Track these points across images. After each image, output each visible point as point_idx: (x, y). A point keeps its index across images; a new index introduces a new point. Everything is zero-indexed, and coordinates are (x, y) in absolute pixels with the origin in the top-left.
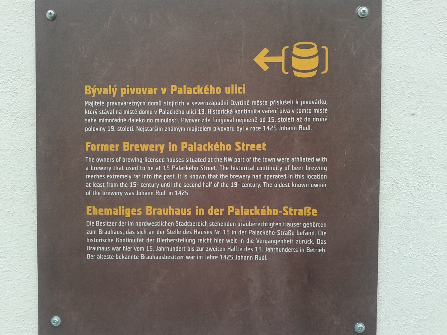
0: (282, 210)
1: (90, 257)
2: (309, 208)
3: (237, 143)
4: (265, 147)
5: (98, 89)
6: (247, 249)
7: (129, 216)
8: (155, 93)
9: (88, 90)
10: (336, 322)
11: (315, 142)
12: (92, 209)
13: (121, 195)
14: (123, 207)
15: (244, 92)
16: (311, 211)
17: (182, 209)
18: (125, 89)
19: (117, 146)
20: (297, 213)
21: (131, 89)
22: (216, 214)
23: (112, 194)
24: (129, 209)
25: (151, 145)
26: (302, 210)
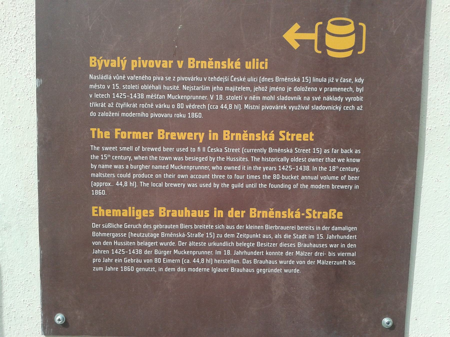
2: (335, 211)
3: (281, 133)
4: (313, 137)
5: (105, 61)
8: (170, 67)
9: (93, 61)
11: (343, 129)
12: (98, 209)
13: (351, 188)
15: (266, 68)
16: (336, 214)
18: (136, 61)
19: (151, 133)
20: (321, 215)
21: (143, 61)
23: (342, 187)
24: (140, 211)
25: (189, 134)
26: (326, 213)
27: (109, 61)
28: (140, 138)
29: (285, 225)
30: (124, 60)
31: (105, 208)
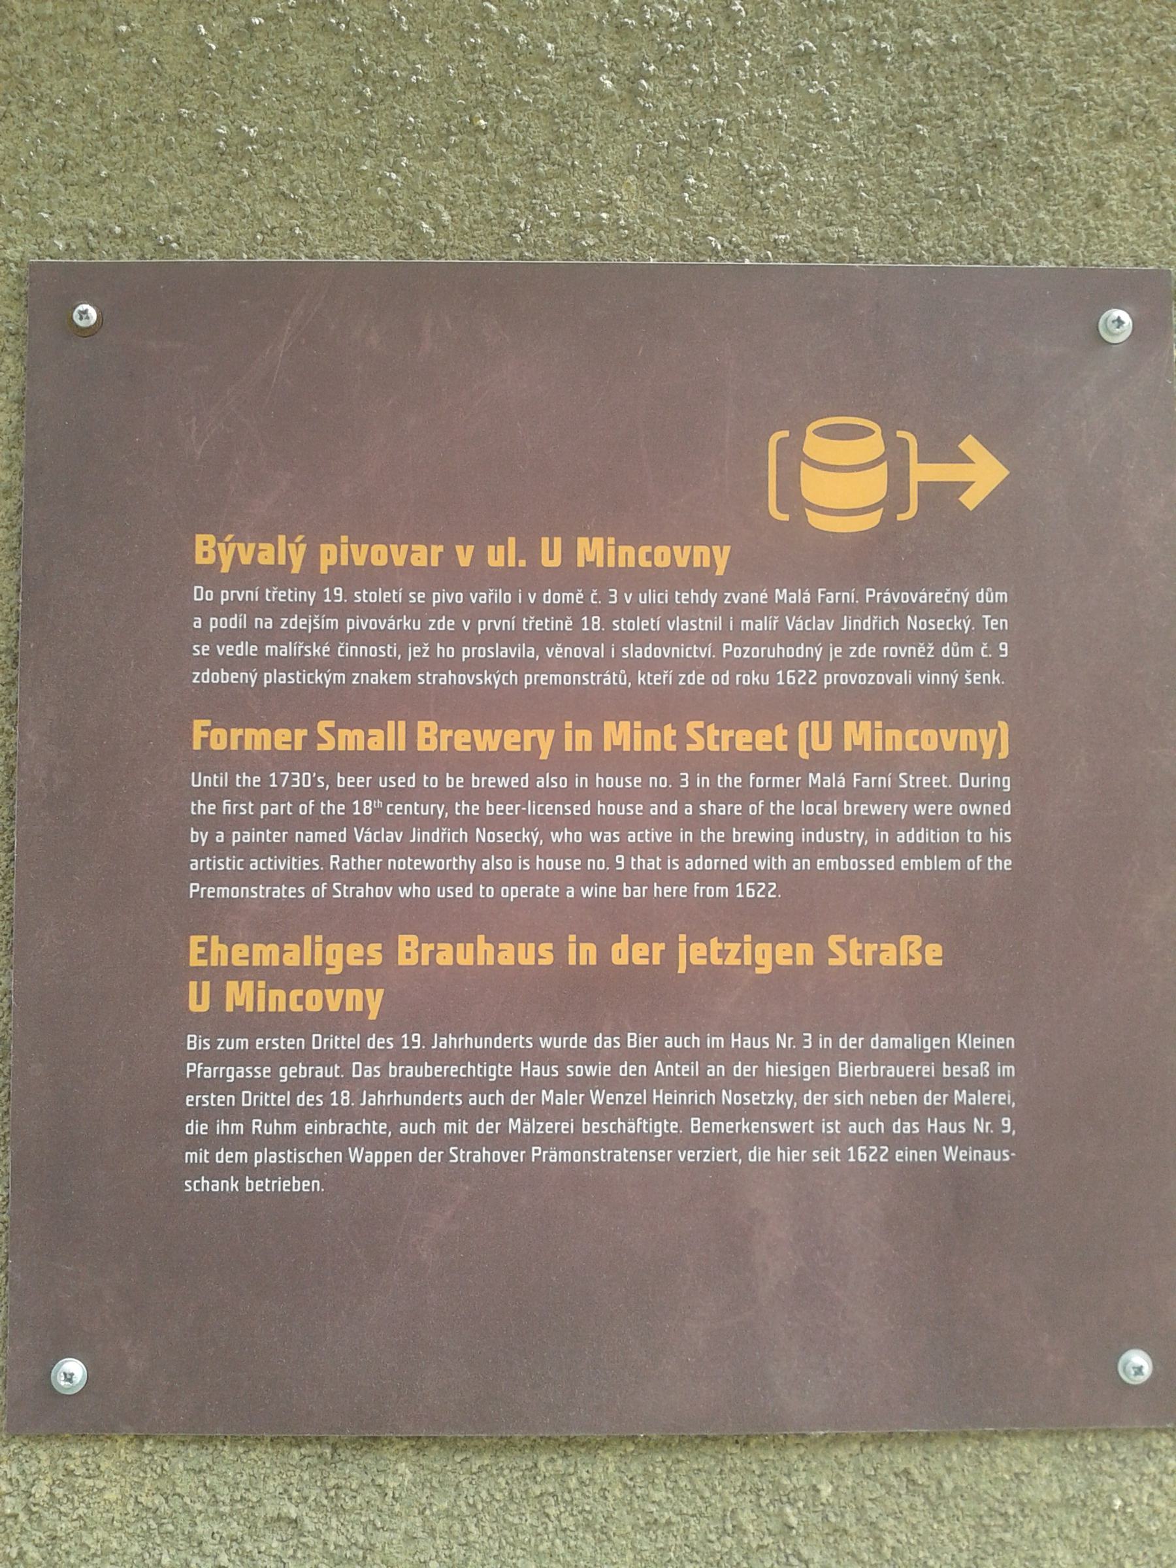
5: (241, 546)
6: (627, 1070)
7: (338, 970)
9: (206, 549)
12: (207, 945)
14: (319, 938)
16: (922, 950)
18: (332, 548)
20: (876, 954)
21: (354, 547)
22: (637, 961)
24: (768, 947)
25: (508, 733)
26: (892, 947)
27: (252, 546)
30: (297, 545)
31: (229, 941)
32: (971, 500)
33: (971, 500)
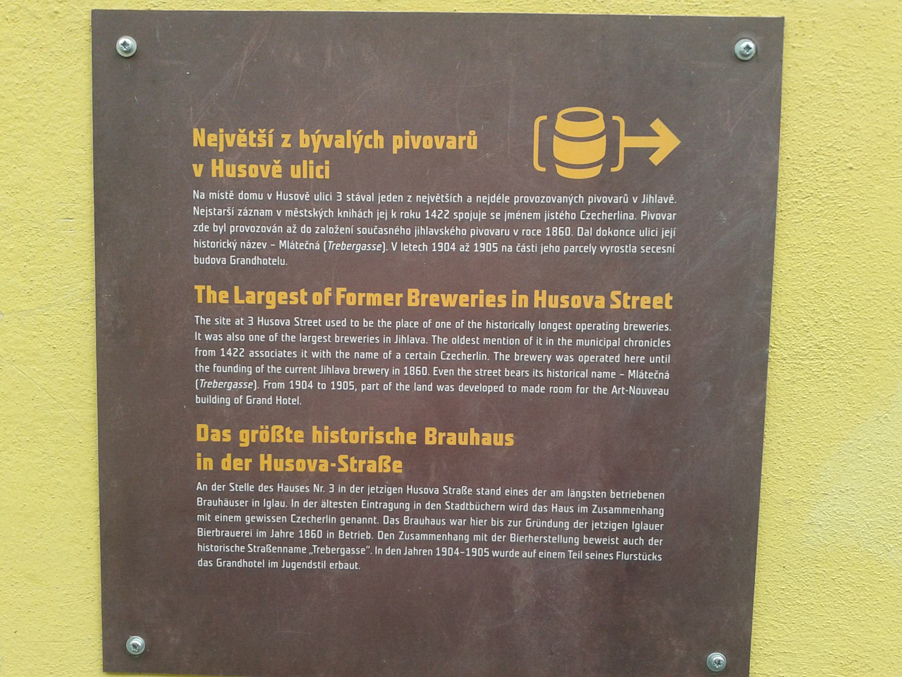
0: (336, 462)
1: (201, 563)
2: (388, 458)
3: (614, 294)
4: (671, 303)
5: (325, 136)
7: (247, 444)
10: (173, 639)
16: (390, 464)
17: (495, 435)
18: (400, 138)
20: (365, 466)
21: (413, 137)
22: (236, 468)
25: (462, 296)
26: (374, 462)
28: (380, 304)
29: (292, 484)
32: (656, 159)
33: (656, 159)
